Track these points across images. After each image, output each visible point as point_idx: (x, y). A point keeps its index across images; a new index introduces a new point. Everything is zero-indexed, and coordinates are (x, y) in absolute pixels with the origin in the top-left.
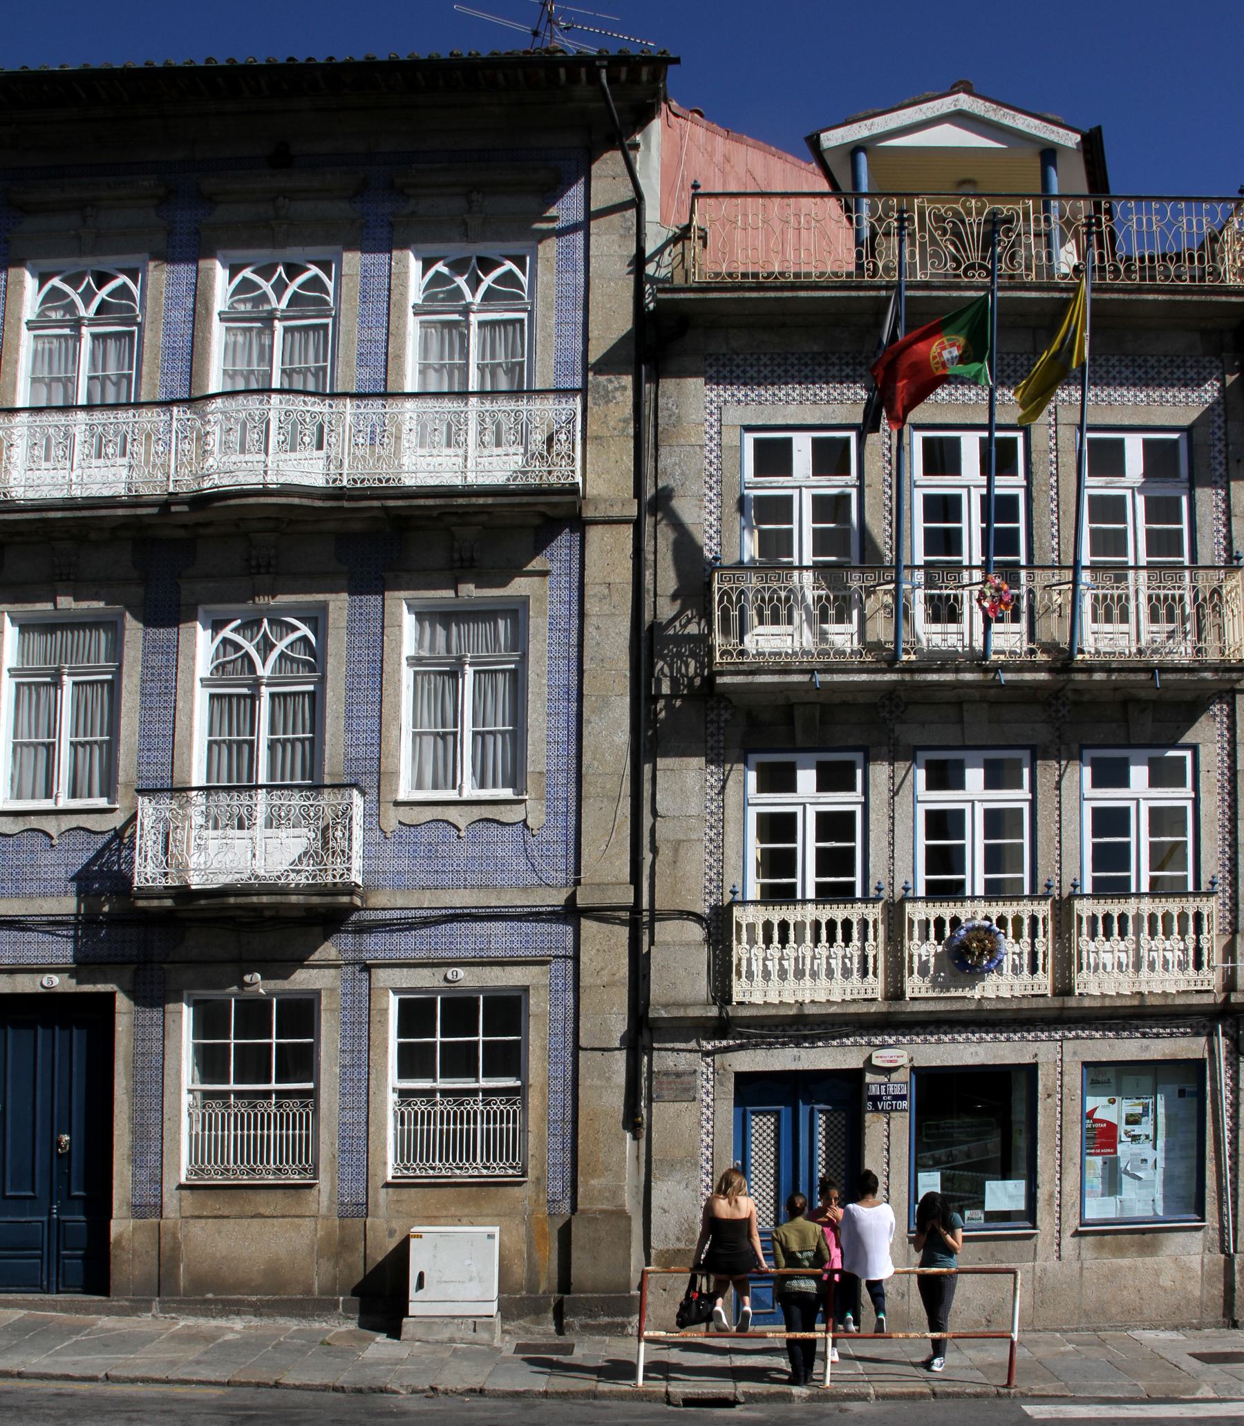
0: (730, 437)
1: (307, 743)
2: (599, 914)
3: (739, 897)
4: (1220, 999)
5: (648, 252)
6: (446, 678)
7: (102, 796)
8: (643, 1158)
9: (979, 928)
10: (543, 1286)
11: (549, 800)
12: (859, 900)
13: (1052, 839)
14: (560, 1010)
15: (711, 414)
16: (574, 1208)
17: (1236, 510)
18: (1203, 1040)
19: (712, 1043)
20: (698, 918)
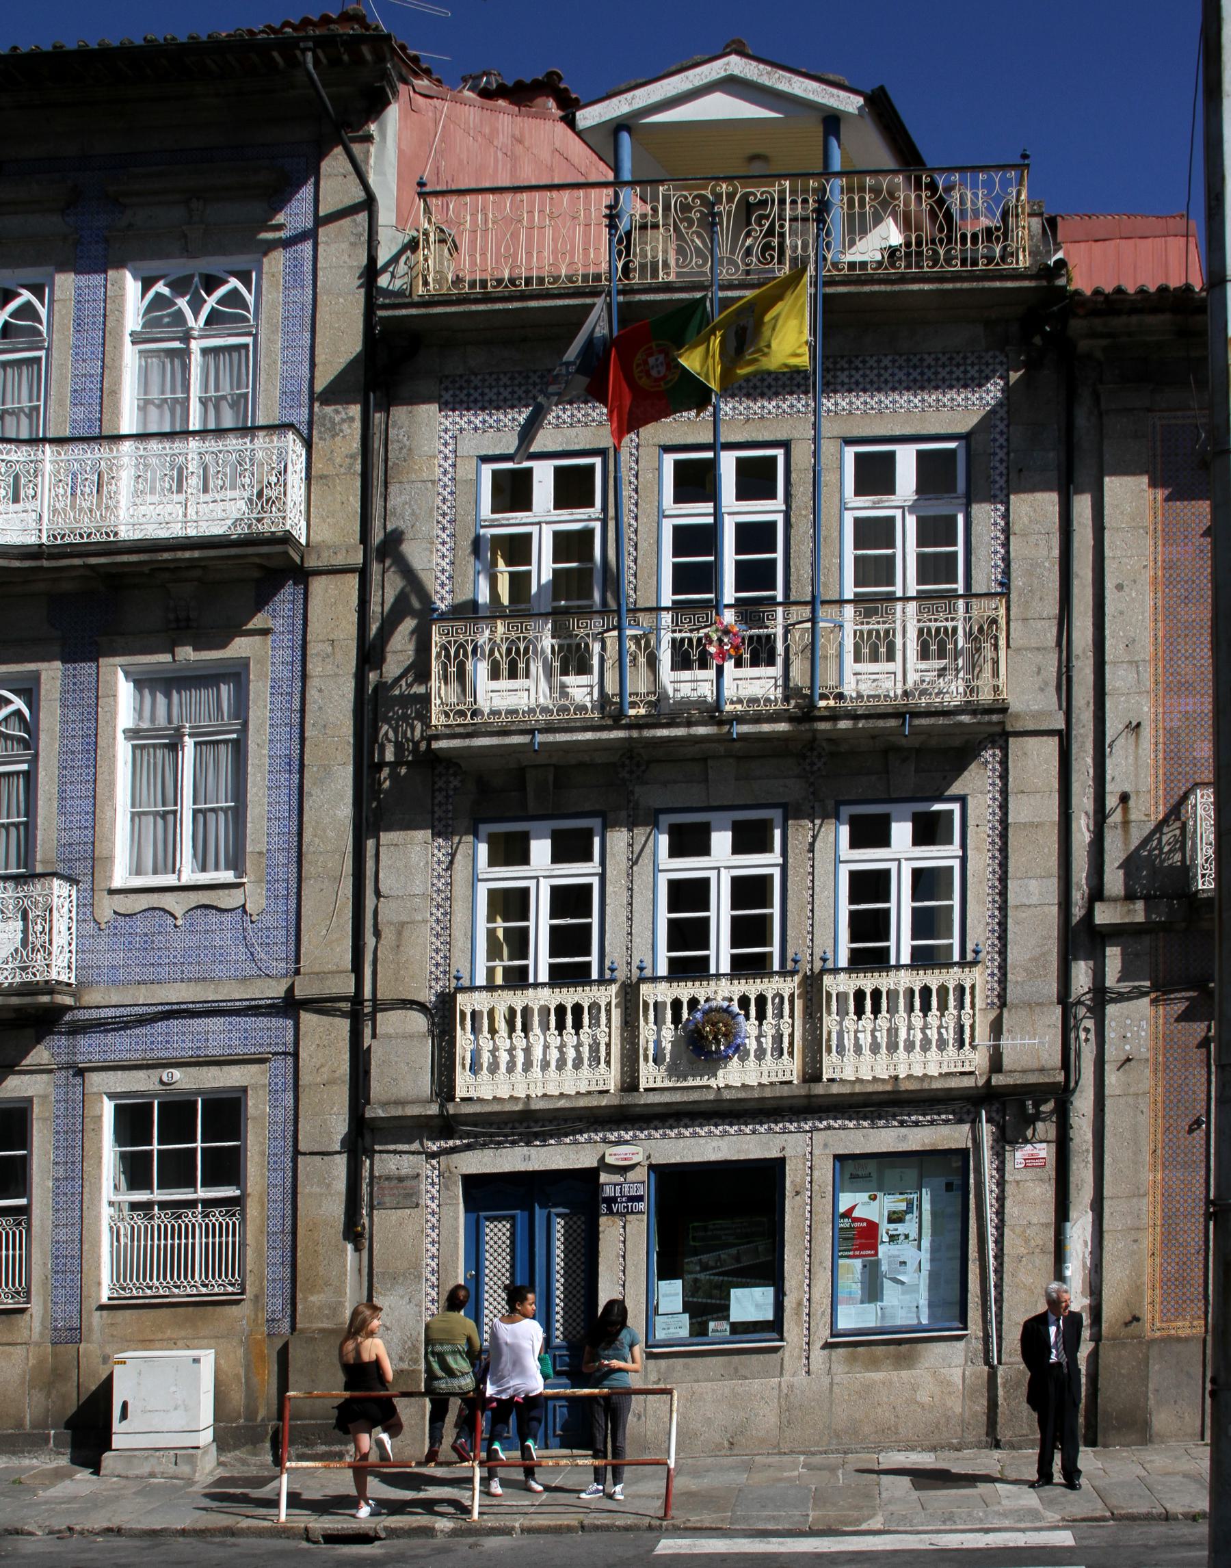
0: (466, 470)
1: (22, 828)
2: (319, 1005)
3: (830, 965)
4: (981, 1082)
5: (381, 263)
6: (166, 751)
7: (227, 868)
8: (365, 1271)
10: (262, 1413)
11: (268, 882)
12: (776, 972)
13: (803, 908)
15: (446, 444)
16: (293, 1327)
17: (1016, 527)
18: (966, 1128)
20: (421, 1007)
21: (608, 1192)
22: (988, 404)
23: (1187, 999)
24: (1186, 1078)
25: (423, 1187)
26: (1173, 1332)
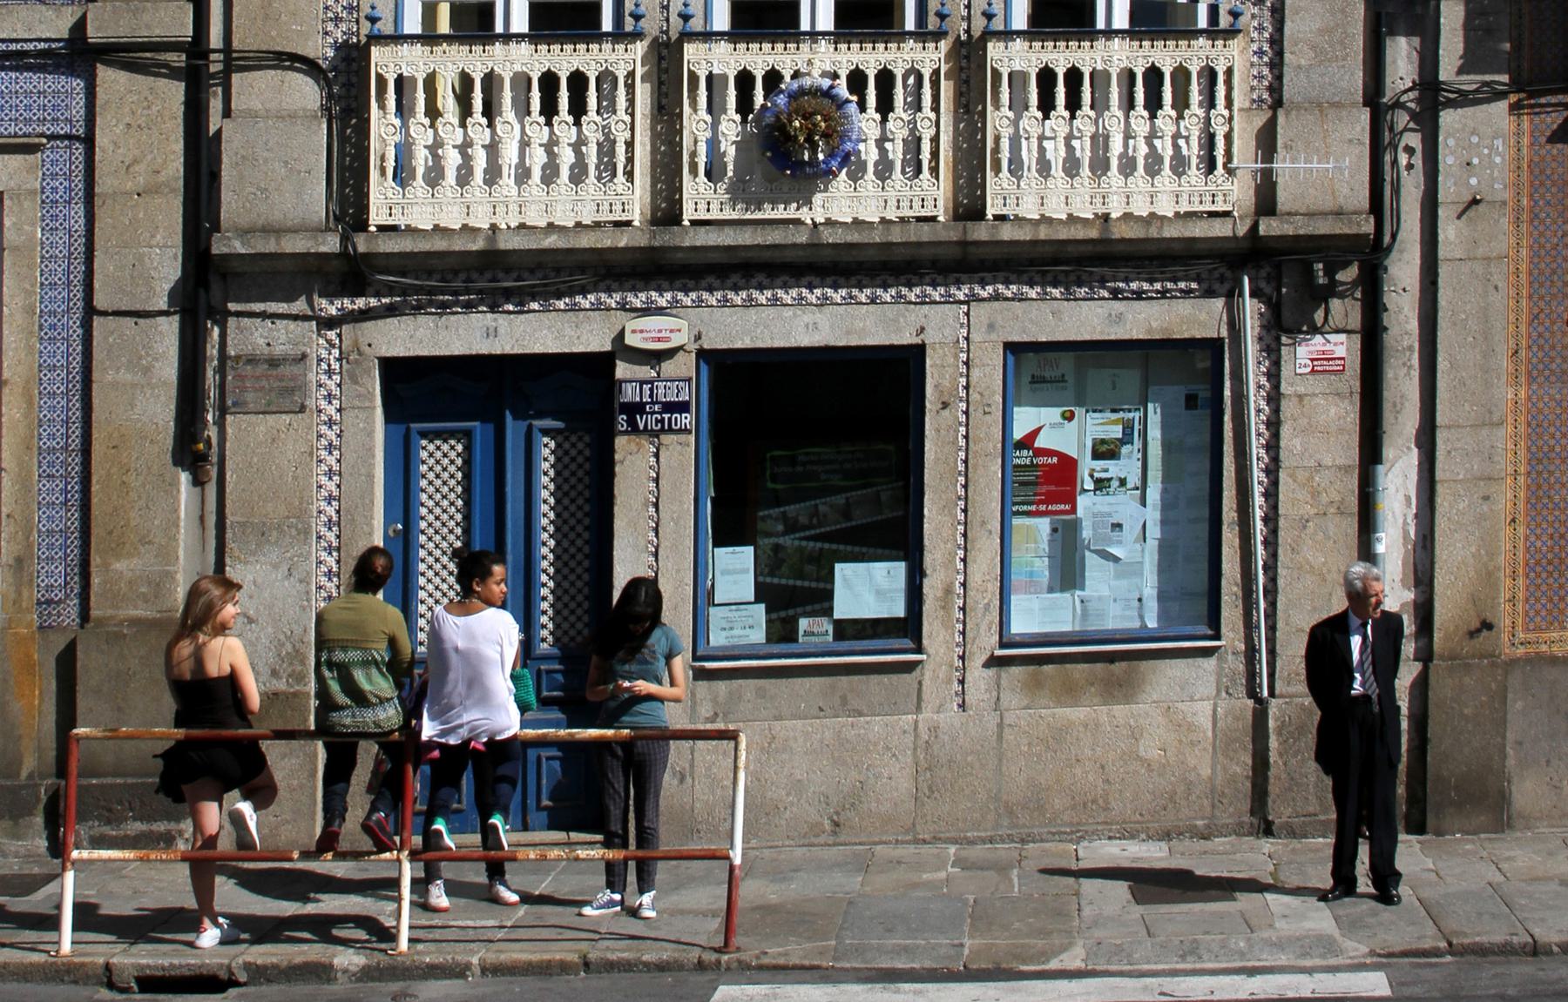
4: (1242, 230)
8: (211, 520)
9: (816, 92)
10: (29, 764)
14: (61, 238)
18: (1219, 304)
19: (338, 303)
20: (310, 66)
21: (630, 394)
25: (312, 377)
26: (1544, 648)
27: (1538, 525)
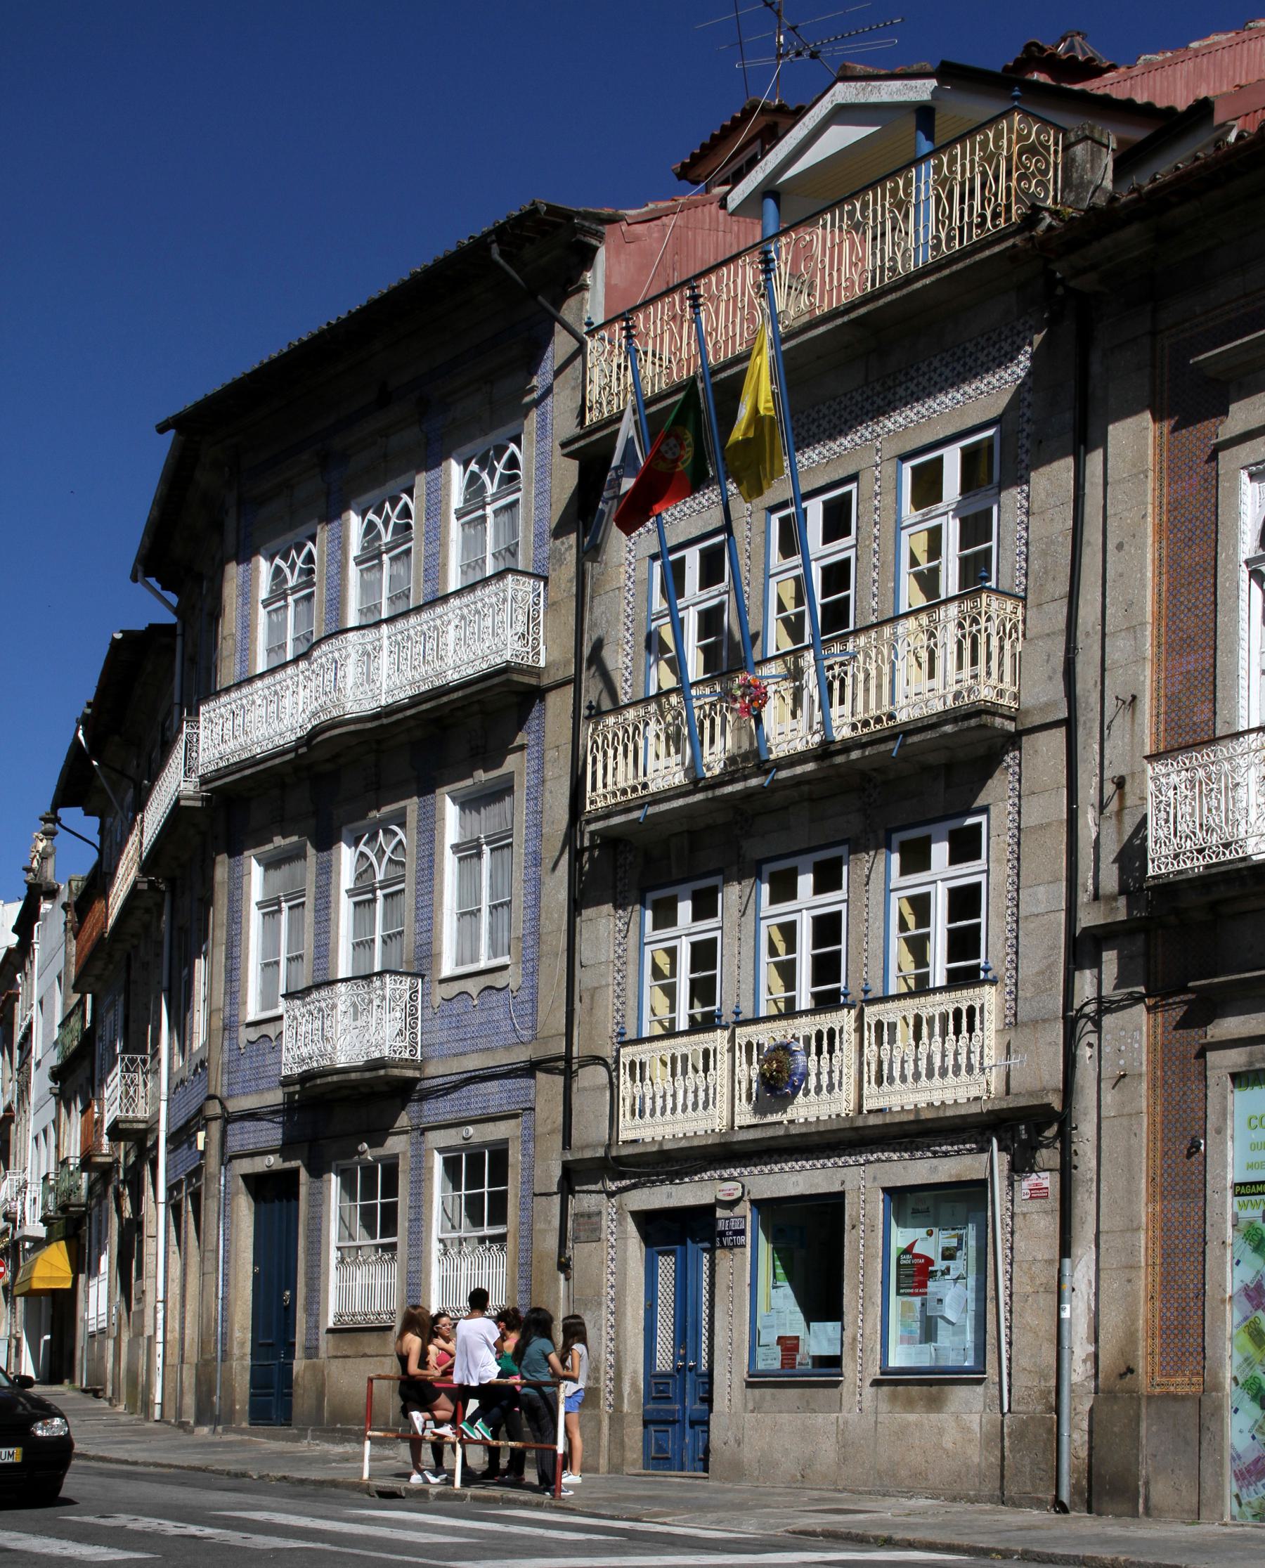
21: (721, 1226)
22: (1019, 377)
23: (1185, 1002)
24: (1184, 1094)
25: (604, 1222)
26: (1172, 1389)
27: (1168, 1301)
